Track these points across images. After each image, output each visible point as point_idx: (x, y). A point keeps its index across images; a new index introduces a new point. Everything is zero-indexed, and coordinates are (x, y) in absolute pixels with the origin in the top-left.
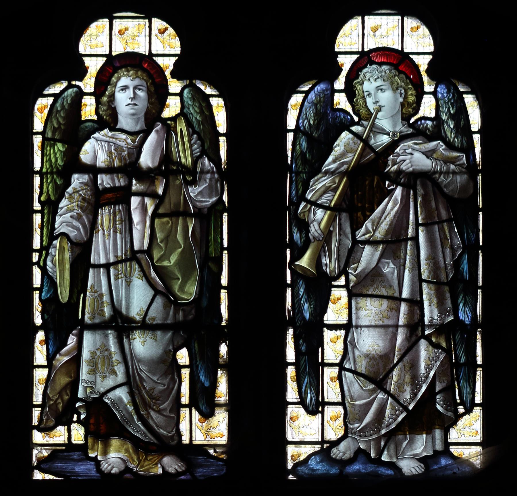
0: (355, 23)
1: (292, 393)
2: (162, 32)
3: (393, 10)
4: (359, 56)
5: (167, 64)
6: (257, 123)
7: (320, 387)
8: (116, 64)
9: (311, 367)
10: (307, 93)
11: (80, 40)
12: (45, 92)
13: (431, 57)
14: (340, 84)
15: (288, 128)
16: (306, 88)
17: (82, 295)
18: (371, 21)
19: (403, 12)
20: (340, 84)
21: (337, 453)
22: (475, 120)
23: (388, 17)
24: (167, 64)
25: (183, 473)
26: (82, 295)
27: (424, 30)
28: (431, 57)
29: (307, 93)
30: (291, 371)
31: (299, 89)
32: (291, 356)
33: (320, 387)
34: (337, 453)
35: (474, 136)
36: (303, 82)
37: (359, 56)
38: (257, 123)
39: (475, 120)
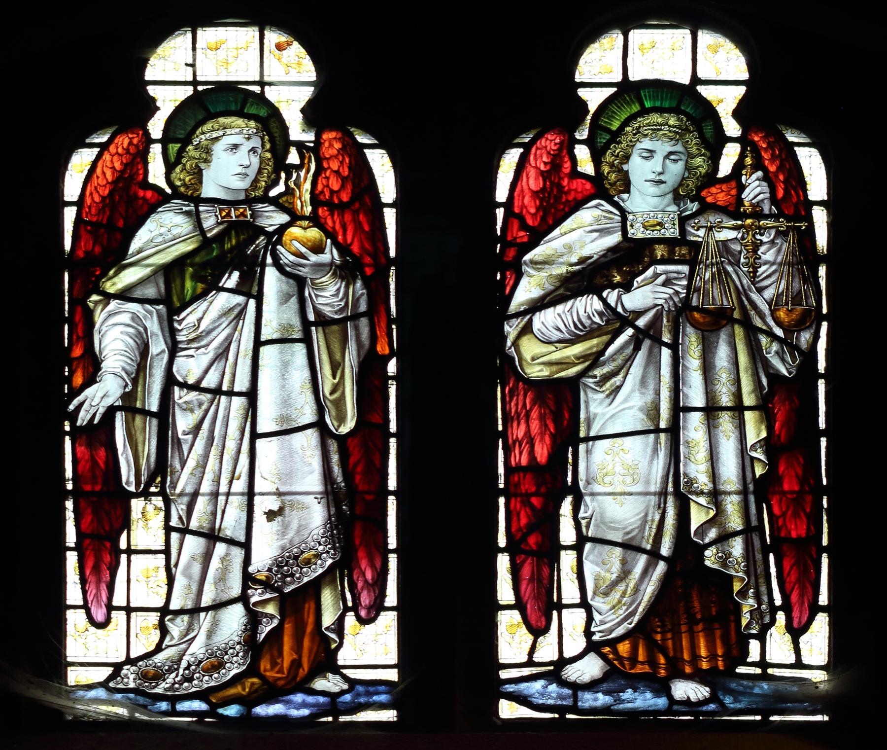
0: (612, 41)
1: (74, 594)
2: (279, 47)
3: (667, 20)
4: (616, 89)
5: (726, 101)
6: (447, 189)
7: (556, 578)
8: (217, 100)
9: (538, 552)
10: (527, 147)
11: (316, 71)
12: (88, 141)
13: (742, 90)
14: (583, 134)
15: (66, 199)
16: (104, 139)
17: (570, 449)
18: (207, 35)
19: (260, 19)
20: (583, 134)
21: (573, 673)
22: (387, 185)
23: (238, 28)
24: (726, 101)
25: (706, 702)
26: (570, 449)
27: (297, 50)
28: (312, 89)
29: (104, 147)
30: (72, 559)
31: (88, 141)
32: (71, 538)
33: (556, 578)
34: (573, 673)
35: (386, 210)
36: (525, 131)
37: (616, 89)
38: (447, 189)
39: (387, 185)
